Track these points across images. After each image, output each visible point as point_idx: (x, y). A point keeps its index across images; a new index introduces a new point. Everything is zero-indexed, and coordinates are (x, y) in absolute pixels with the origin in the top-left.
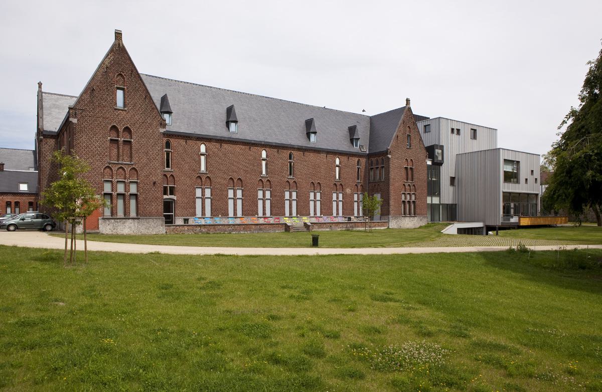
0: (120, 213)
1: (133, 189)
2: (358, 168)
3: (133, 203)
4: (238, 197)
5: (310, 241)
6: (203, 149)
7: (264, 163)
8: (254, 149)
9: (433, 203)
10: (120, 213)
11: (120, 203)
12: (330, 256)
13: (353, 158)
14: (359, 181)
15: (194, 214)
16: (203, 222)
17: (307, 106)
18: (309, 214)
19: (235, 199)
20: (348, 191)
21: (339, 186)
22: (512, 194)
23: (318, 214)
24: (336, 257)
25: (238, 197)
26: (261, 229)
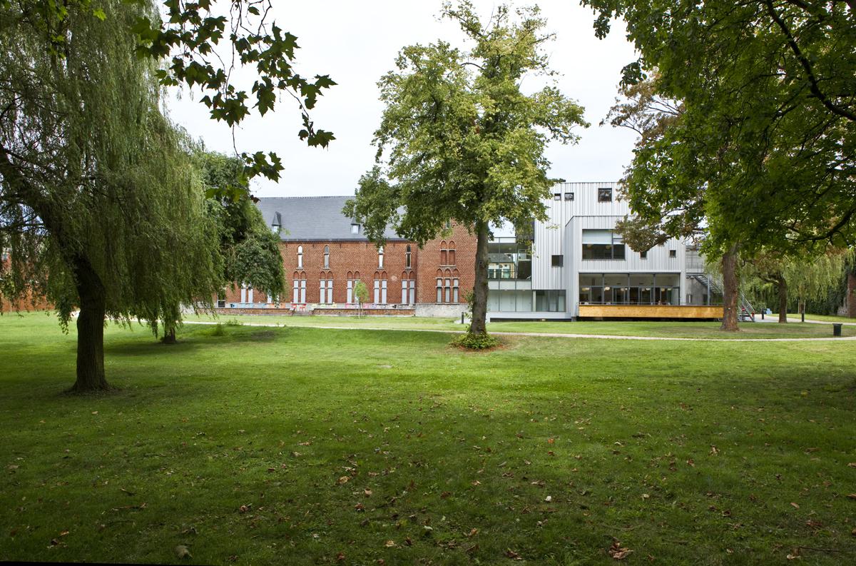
0: (447, 299)
1: (456, 284)
2: (409, 255)
3: (456, 292)
4: (411, 287)
5: (832, 331)
6: (300, 249)
7: (300, 257)
8: (292, 246)
9: (501, 289)
10: (447, 299)
11: (448, 292)
12: (605, 339)
13: (401, 245)
14: (410, 268)
15: (239, 301)
16: (247, 306)
17: (275, 198)
18: (346, 301)
19: (326, 288)
20: (394, 278)
21: (384, 274)
22: (605, 275)
23: (330, 300)
24: (346, 334)
25: (411, 287)
26: (268, 313)
